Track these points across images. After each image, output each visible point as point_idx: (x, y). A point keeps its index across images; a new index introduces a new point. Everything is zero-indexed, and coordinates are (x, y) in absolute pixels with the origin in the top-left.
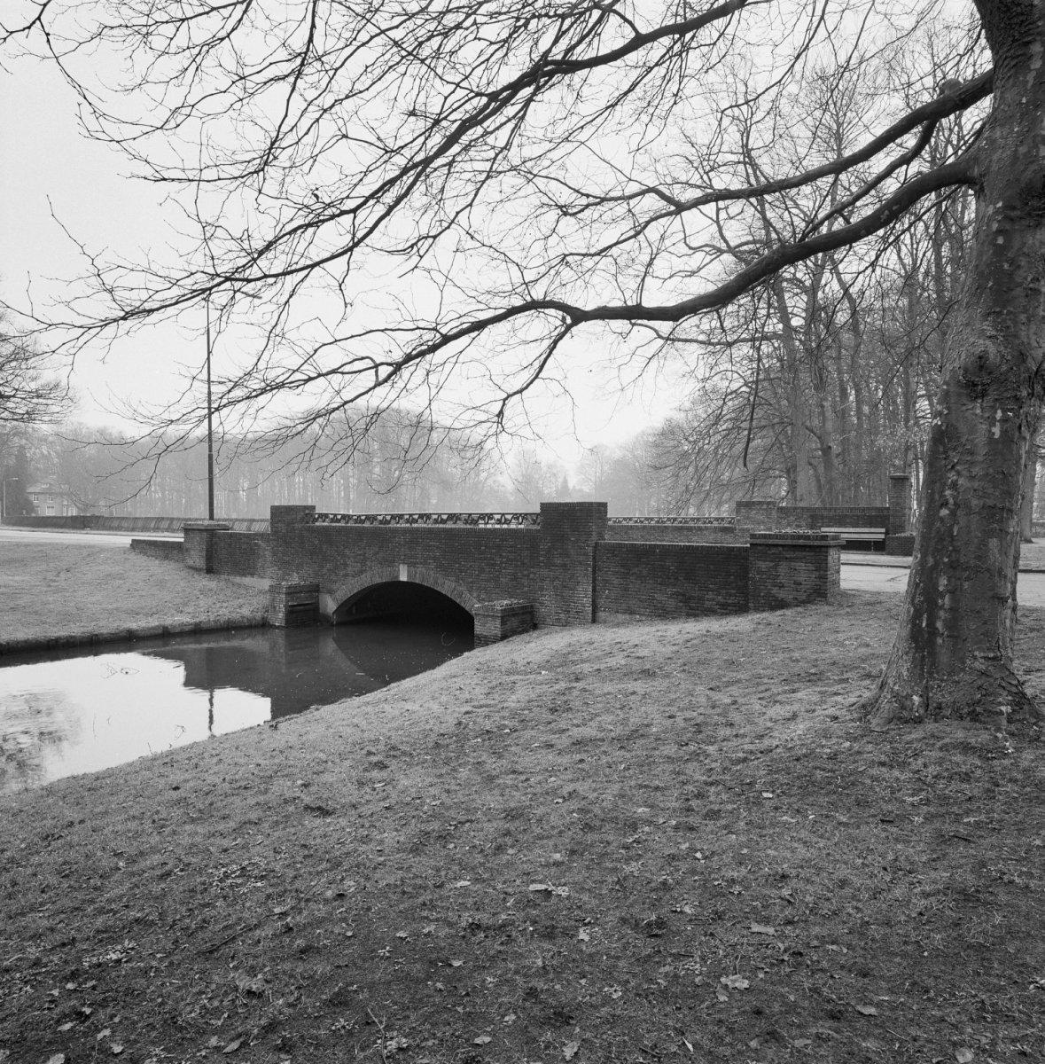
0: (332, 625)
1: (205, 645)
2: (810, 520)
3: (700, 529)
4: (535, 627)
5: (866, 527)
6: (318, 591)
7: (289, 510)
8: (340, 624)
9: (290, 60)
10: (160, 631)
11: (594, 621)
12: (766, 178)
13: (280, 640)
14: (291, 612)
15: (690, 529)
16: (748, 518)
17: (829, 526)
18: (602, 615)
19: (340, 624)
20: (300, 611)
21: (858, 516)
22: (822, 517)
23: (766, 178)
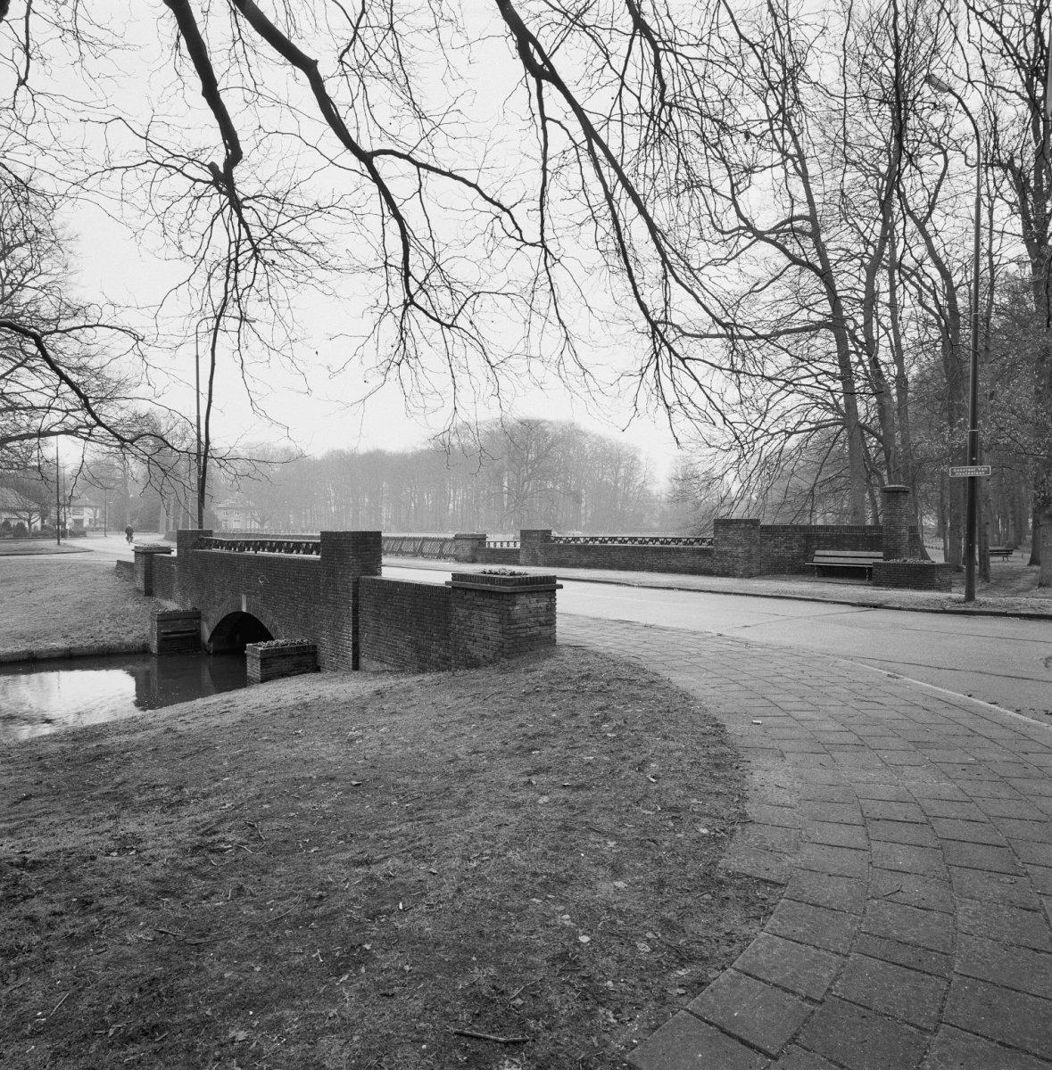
0: (209, 653)
1: (274, 643)
2: (804, 541)
3: (678, 550)
4: (317, 670)
5: (865, 550)
6: (199, 618)
7: (332, 534)
8: (216, 653)
9: (844, 45)
10: (25, 657)
11: (356, 667)
12: (1020, 73)
13: (154, 660)
14: (164, 641)
15: (669, 551)
16: (726, 539)
17: (824, 549)
18: (363, 661)
19: (216, 653)
20: (175, 638)
21: (856, 536)
22: (819, 538)
23: (1020, 73)
